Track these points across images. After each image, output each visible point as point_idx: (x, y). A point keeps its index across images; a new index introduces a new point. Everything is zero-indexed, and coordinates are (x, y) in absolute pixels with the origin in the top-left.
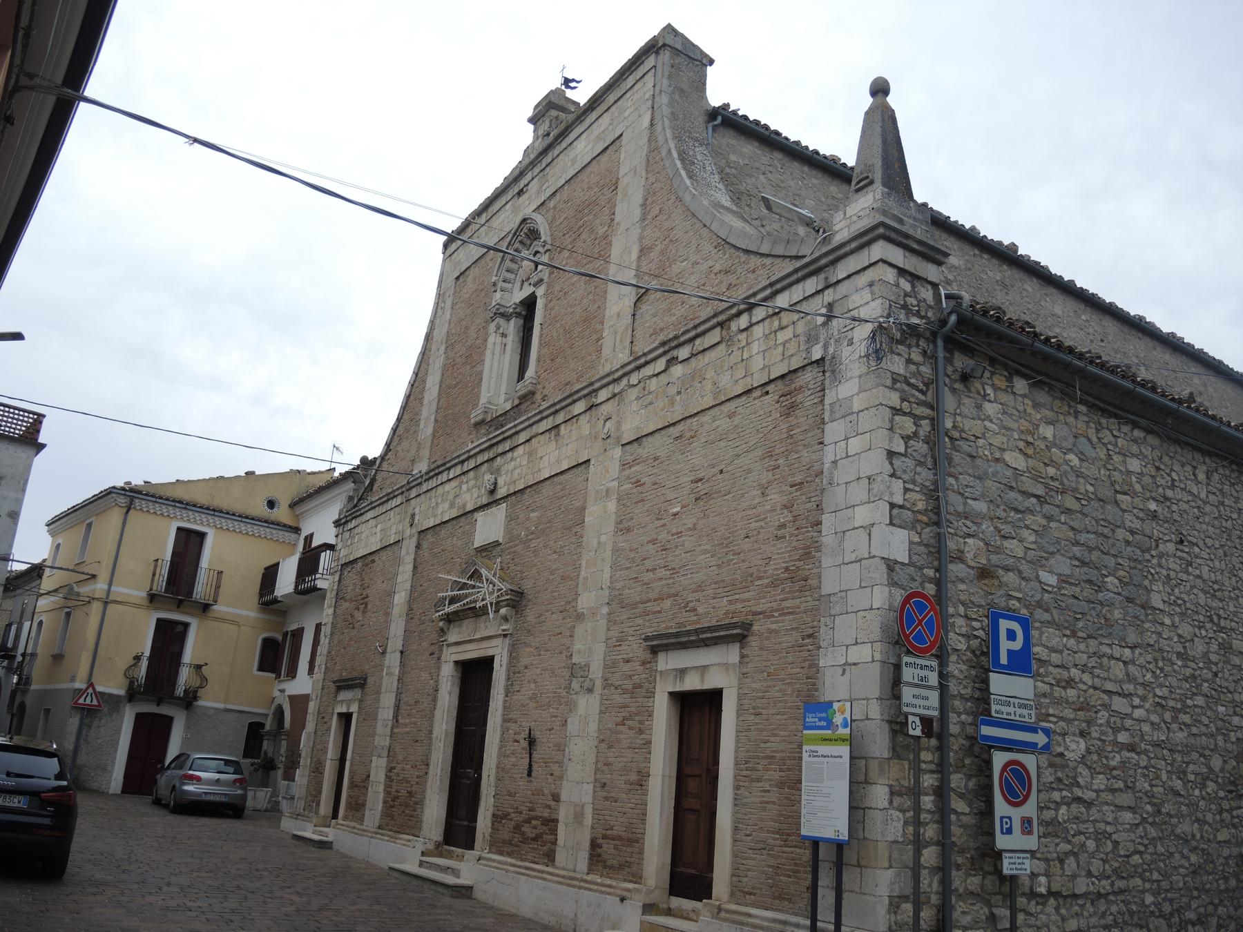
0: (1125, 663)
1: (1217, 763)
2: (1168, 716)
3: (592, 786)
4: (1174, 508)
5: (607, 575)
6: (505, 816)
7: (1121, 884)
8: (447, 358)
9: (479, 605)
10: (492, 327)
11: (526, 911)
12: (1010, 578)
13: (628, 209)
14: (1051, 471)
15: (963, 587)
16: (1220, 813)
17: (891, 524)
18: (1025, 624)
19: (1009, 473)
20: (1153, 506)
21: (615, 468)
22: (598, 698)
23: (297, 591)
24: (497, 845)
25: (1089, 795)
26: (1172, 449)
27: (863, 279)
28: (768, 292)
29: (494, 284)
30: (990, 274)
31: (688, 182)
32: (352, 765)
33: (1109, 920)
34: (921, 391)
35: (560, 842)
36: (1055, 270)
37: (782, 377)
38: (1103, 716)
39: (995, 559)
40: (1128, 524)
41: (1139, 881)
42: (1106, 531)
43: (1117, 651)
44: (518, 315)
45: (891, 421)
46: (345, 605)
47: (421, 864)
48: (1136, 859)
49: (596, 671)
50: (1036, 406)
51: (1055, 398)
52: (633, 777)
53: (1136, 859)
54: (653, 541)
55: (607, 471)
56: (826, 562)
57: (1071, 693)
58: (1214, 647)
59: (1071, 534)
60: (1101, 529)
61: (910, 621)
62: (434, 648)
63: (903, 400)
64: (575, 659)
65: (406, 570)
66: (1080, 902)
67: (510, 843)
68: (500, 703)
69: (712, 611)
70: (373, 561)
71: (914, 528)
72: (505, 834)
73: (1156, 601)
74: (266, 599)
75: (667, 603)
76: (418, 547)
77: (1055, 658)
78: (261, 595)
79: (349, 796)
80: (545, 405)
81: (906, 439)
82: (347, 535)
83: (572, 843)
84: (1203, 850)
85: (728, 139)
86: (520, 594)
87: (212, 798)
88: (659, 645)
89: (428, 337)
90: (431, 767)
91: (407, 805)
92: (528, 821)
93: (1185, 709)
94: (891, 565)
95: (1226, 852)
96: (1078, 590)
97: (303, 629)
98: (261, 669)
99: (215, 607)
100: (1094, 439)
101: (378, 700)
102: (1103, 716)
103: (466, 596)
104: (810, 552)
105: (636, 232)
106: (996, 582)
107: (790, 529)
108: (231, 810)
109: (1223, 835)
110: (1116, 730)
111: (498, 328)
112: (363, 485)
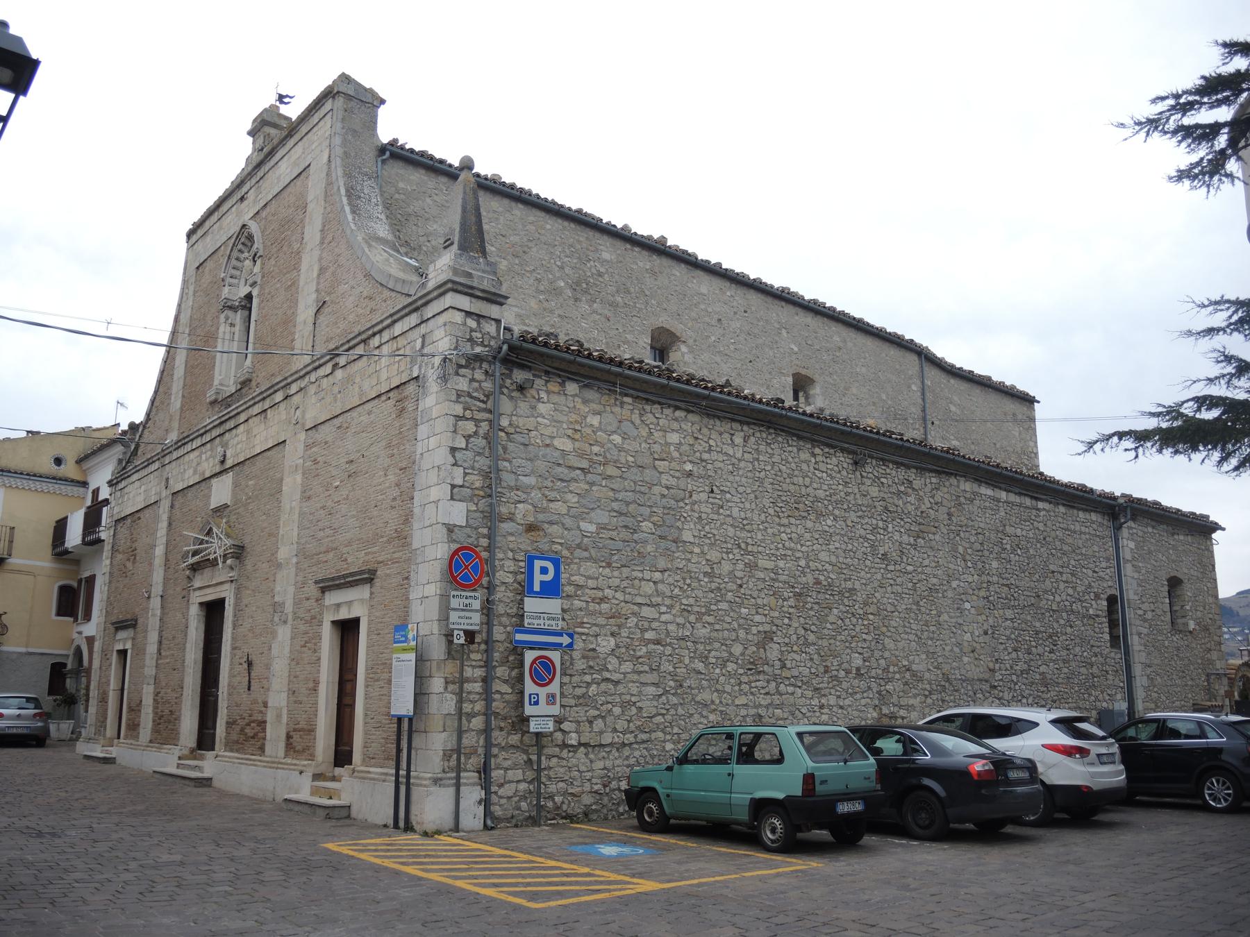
0: (655, 583)
1: (737, 649)
2: (692, 618)
4: (709, 466)
5: (295, 533)
6: (234, 722)
7: (644, 737)
9: (211, 557)
10: (222, 317)
11: (245, 791)
12: (554, 529)
13: (312, 232)
14: (596, 449)
15: (512, 539)
16: (739, 684)
17: (452, 499)
18: (556, 563)
19: (557, 454)
20: (688, 467)
21: (301, 447)
23: (84, 543)
24: (231, 745)
25: (615, 677)
26: (712, 422)
27: (441, 320)
28: (389, 321)
30: (641, 264)
31: (350, 217)
33: (632, 761)
34: (483, 402)
35: (268, 737)
36: (702, 256)
37: (398, 387)
38: (632, 621)
39: (541, 517)
40: (664, 482)
41: (660, 734)
42: (643, 489)
43: (647, 575)
45: (455, 426)
46: (120, 556)
47: (178, 766)
48: (659, 719)
49: (289, 608)
50: (585, 402)
51: (603, 394)
52: (311, 685)
53: (659, 719)
54: (323, 508)
55: (294, 454)
56: (416, 526)
57: (605, 606)
58: (740, 566)
59: (611, 494)
60: (638, 488)
61: (458, 566)
62: (185, 593)
63: (465, 409)
64: (277, 599)
65: (163, 525)
66: (607, 749)
67: (237, 742)
68: (229, 635)
69: (356, 561)
71: (472, 500)
72: (234, 736)
73: (687, 536)
74: (59, 550)
75: (331, 555)
77: (591, 583)
78: (55, 546)
79: (128, 719)
80: (258, 391)
81: (467, 438)
82: (118, 493)
83: (275, 735)
84: (721, 712)
85: (396, 170)
87: (15, 731)
88: (327, 586)
91: (170, 722)
92: (248, 724)
93: (708, 613)
94: (450, 529)
95: (743, 712)
96: (615, 533)
98: (59, 614)
99: (10, 560)
100: (638, 422)
101: (145, 637)
102: (632, 621)
103: (206, 549)
104: (407, 519)
105: (317, 253)
106: (541, 533)
107: (398, 502)
108: (34, 740)
109: (742, 700)
110: (643, 631)
111: (227, 318)
112: (128, 448)
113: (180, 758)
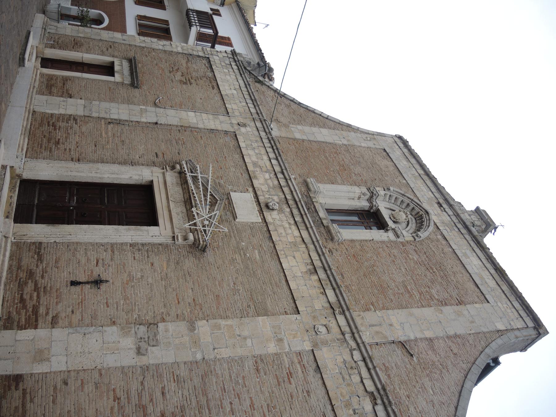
3: (65, 369)
8: (340, 146)
10: (364, 190)
22: (132, 362)
23: (188, 11)
24: (19, 247)
28: (253, 98)
29: (389, 189)
32: (78, 78)
44: (371, 207)
46: (184, 62)
67: (19, 267)
70: (213, 88)
76: (226, 132)
79: (57, 77)
82: (228, 62)
86: (204, 250)
88: (132, 63)
89: (349, 127)
90: (77, 165)
91: (49, 140)
92: (36, 289)
97: (165, 10)
111: (364, 194)
113: (12, 167)
